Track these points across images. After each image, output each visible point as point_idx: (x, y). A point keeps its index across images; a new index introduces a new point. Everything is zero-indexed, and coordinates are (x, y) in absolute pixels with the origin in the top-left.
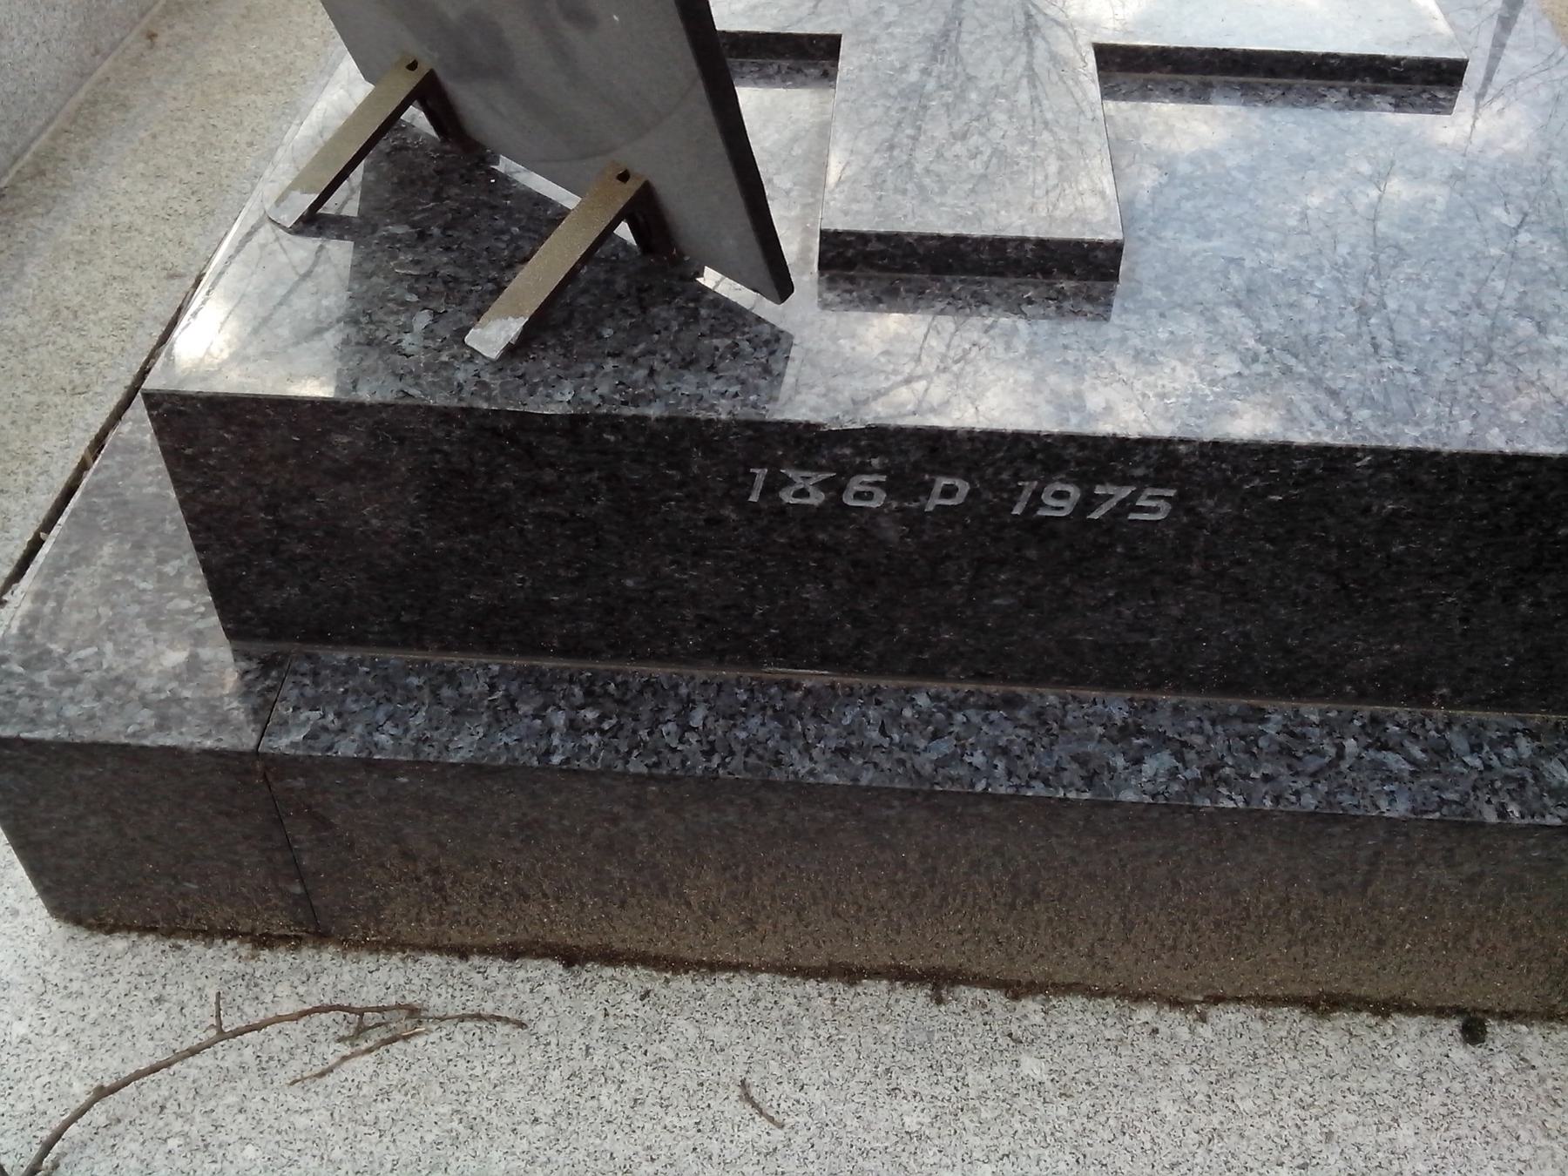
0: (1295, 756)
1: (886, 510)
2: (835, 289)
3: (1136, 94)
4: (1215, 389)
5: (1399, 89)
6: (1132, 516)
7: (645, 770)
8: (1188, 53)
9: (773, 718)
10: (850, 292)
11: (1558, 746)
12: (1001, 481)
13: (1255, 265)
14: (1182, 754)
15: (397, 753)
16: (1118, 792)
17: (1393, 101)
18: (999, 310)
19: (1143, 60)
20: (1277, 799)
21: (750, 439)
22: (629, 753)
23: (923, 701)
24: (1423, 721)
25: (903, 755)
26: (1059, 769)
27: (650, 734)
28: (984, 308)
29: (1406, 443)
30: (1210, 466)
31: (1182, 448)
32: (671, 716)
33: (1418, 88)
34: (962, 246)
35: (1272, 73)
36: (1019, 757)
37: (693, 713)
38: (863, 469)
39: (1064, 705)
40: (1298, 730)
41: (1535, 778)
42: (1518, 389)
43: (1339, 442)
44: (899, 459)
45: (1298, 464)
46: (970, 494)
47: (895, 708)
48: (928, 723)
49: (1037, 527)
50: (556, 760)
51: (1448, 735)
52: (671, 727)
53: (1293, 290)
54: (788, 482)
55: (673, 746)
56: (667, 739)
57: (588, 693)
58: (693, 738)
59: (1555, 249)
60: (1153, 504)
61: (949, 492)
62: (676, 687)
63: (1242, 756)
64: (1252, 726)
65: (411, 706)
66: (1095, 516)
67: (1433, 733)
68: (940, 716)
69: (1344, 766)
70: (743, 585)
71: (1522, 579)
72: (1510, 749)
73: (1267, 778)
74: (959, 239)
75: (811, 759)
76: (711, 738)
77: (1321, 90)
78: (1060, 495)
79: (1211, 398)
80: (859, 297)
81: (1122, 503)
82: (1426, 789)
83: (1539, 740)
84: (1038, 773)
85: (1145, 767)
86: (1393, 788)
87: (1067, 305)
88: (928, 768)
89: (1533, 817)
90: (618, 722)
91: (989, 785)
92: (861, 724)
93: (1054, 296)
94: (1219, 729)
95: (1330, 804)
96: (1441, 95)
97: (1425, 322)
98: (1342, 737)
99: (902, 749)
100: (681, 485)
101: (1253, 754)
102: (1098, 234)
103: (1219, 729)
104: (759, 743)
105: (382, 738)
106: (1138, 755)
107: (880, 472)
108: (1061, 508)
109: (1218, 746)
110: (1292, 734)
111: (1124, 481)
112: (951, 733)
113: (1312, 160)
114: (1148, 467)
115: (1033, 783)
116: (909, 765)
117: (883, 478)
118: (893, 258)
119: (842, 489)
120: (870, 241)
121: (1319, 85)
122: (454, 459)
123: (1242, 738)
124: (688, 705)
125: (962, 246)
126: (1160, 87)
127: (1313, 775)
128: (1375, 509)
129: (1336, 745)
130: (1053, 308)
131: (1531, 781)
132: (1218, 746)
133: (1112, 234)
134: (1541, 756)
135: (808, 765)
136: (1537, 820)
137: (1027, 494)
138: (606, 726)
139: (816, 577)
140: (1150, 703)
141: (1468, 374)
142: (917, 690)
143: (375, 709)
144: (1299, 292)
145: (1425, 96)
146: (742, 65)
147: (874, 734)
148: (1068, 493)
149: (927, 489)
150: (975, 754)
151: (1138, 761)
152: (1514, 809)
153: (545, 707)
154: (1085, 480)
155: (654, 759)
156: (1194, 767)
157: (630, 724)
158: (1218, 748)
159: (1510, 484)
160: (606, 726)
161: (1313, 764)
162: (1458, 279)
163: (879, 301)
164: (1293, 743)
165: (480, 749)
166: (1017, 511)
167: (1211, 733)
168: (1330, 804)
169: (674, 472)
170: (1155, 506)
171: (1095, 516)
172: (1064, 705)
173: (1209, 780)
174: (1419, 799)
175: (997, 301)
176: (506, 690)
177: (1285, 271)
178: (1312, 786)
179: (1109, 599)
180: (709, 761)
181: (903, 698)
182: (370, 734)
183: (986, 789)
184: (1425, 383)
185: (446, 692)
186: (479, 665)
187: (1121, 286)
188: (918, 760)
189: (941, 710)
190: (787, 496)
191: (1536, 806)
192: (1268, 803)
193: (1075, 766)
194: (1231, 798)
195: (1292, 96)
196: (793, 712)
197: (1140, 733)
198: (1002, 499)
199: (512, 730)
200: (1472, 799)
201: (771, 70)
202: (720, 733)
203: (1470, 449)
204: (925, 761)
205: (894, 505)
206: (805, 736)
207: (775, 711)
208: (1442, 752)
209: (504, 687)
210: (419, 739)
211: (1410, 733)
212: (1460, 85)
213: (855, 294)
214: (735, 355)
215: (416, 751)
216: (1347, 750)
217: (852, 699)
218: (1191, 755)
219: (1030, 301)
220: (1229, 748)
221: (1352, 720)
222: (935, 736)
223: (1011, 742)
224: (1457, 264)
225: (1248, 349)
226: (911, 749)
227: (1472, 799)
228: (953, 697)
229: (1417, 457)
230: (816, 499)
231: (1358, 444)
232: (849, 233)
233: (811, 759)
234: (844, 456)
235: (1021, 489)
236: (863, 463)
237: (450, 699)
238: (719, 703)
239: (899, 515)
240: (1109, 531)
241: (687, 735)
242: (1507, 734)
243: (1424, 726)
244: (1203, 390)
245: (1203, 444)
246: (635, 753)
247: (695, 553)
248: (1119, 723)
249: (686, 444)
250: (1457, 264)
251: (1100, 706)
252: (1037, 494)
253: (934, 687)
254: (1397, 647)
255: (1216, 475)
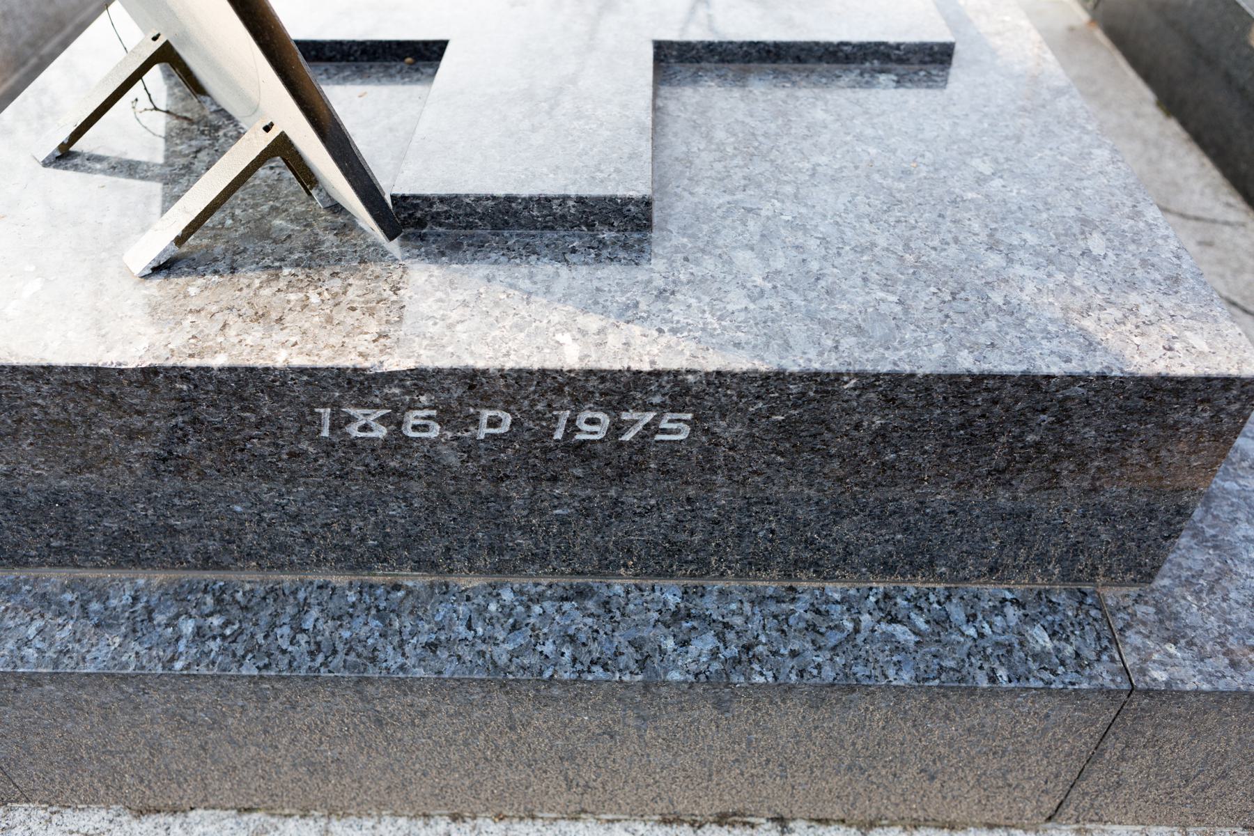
0: (818, 632)
1: (443, 440)
2: (407, 245)
3: (689, 79)
4: (723, 323)
5: (901, 69)
6: (659, 437)
7: (256, 672)
8: (730, 46)
9: (374, 617)
10: (419, 248)
11: (1041, 613)
12: (538, 412)
13: (770, 214)
14: (724, 634)
15: (38, 666)
16: (666, 673)
17: (895, 78)
18: (546, 260)
19: (694, 52)
20: (801, 673)
21: (307, 383)
22: (244, 657)
23: (507, 596)
24: (927, 595)
25: (484, 647)
26: (618, 654)
27: (266, 637)
28: (534, 257)
29: (884, 368)
30: (717, 392)
31: (690, 378)
32: (287, 620)
33: (917, 67)
34: (513, 205)
35: (798, 60)
36: (584, 644)
37: (307, 616)
38: (412, 406)
39: (628, 593)
40: (823, 608)
41: (1021, 644)
42: (987, 314)
43: (827, 368)
44: (444, 396)
45: (794, 388)
46: (513, 424)
47: (483, 603)
48: (510, 615)
49: (582, 451)
50: (178, 665)
51: (948, 607)
52: (286, 630)
53: (800, 233)
54: (350, 419)
55: (284, 647)
56: (280, 641)
57: (219, 601)
58: (302, 638)
59: (1024, 191)
60: (674, 426)
61: (494, 423)
62: (294, 593)
63: (775, 634)
64: (784, 606)
65: (60, 621)
66: (627, 437)
67: (935, 605)
68: (520, 609)
69: (859, 639)
70: (337, 507)
71: (999, 478)
72: (999, 618)
73: (794, 654)
74: (510, 199)
75: (403, 654)
76: (319, 638)
77: (837, 72)
78: (591, 422)
79: (719, 331)
80: (426, 251)
81: (647, 426)
82: (928, 657)
83: (1025, 609)
84: (599, 658)
85: (691, 648)
86: (899, 658)
87: (605, 253)
88: (505, 658)
89: (1018, 680)
90: (240, 628)
91: (555, 671)
92: (451, 619)
93: (596, 245)
94: (757, 609)
95: (846, 676)
96: (934, 72)
97: (910, 258)
98: (859, 613)
99: (484, 641)
100: (258, 426)
101: (783, 631)
102: (629, 190)
103: (757, 609)
104: (360, 641)
105: (30, 652)
106: (686, 638)
107: (430, 408)
108: (596, 433)
109: (755, 626)
110: (818, 612)
111: (647, 408)
112: (527, 625)
113: (826, 127)
114: (664, 395)
115: (594, 668)
116: (488, 656)
117: (434, 413)
118: (457, 216)
119: (400, 424)
120: (434, 203)
121: (836, 69)
122: (51, 411)
123: (775, 617)
124: (304, 608)
125: (513, 205)
126: (709, 74)
127: (834, 648)
128: (865, 424)
129: (853, 620)
130: (593, 256)
131: (1017, 647)
132: (755, 626)
133: (640, 189)
134: (1025, 623)
135: (400, 660)
136: (1023, 684)
137: (563, 422)
138: (228, 632)
139: (397, 498)
140: (700, 589)
141: (944, 302)
142: (502, 586)
143: (28, 625)
144: (805, 234)
145: (922, 73)
146: (371, 67)
147: (461, 629)
148: (599, 420)
149: (476, 421)
150: (547, 643)
151: (685, 643)
152: (1002, 673)
153: (177, 616)
154: (613, 408)
155: (266, 661)
156: (733, 647)
157: (248, 626)
158: (755, 627)
159: (980, 399)
160: (228, 632)
161: (834, 638)
162: (940, 220)
163: (443, 254)
164: (818, 620)
165: (114, 659)
166: (558, 435)
167: (749, 614)
168: (846, 676)
169: (248, 414)
170: (675, 427)
171: (627, 437)
172: (628, 593)
173: (744, 658)
174: (922, 666)
175: (545, 251)
176: (148, 602)
177: (794, 218)
178: (831, 659)
179: (652, 507)
180: (313, 660)
181: (490, 594)
182: (19, 648)
183: (552, 676)
184: (906, 311)
185: (95, 606)
186: (128, 579)
187: (655, 235)
188: (497, 651)
189: (521, 603)
190: (354, 431)
191: (1021, 670)
192: (794, 677)
193: (631, 650)
194: (762, 674)
195: (814, 78)
196: (393, 611)
197: (689, 616)
198: (542, 427)
199: (145, 639)
200: (967, 665)
201: (393, 71)
202: (327, 633)
203: (941, 370)
204: (501, 654)
205: (449, 434)
206: (401, 633)
207: (378, 611)
208: (943, 622)
209: (145, 599)
210: (61, 652)
211: (916, 606)
212: (950, 64)
213: (423, 249)
214: (304, 307)
215: (56, 663)
216: (863, 624)
217: (446, 596)
218: (731, 636)
219: (574, 251)
220: (764, 627)
221: (868, 597)
222: (514, 627)
223: (578, 630)
224: (939, 207)
225: (756, 286)
226: (492, 641)
227: (967, 665)
228: (533, 591)
229: (896, 379)
230: (381, 432)
231: (843, 369)
232: (415, 197)
233: (403, 654)
234: (395, 395)
235: (557, 418)
236: (413, 401)
237: (96, 612)
238: (331, 605)
239: (455, 443)
240: (641, 451)
241: (299, 636)
242: (997, 604)
243: (928, 599)
244: (712, 324)
245: (707, 374)
246: (250, 656)
247: (287, 481)
248: (673, 608)
249: (251, 390)
250: (939, 207)
251: (658, 593)
252: (571, 422)
253: (516, 582)
254: (899, 536)
255: (723, 399)
